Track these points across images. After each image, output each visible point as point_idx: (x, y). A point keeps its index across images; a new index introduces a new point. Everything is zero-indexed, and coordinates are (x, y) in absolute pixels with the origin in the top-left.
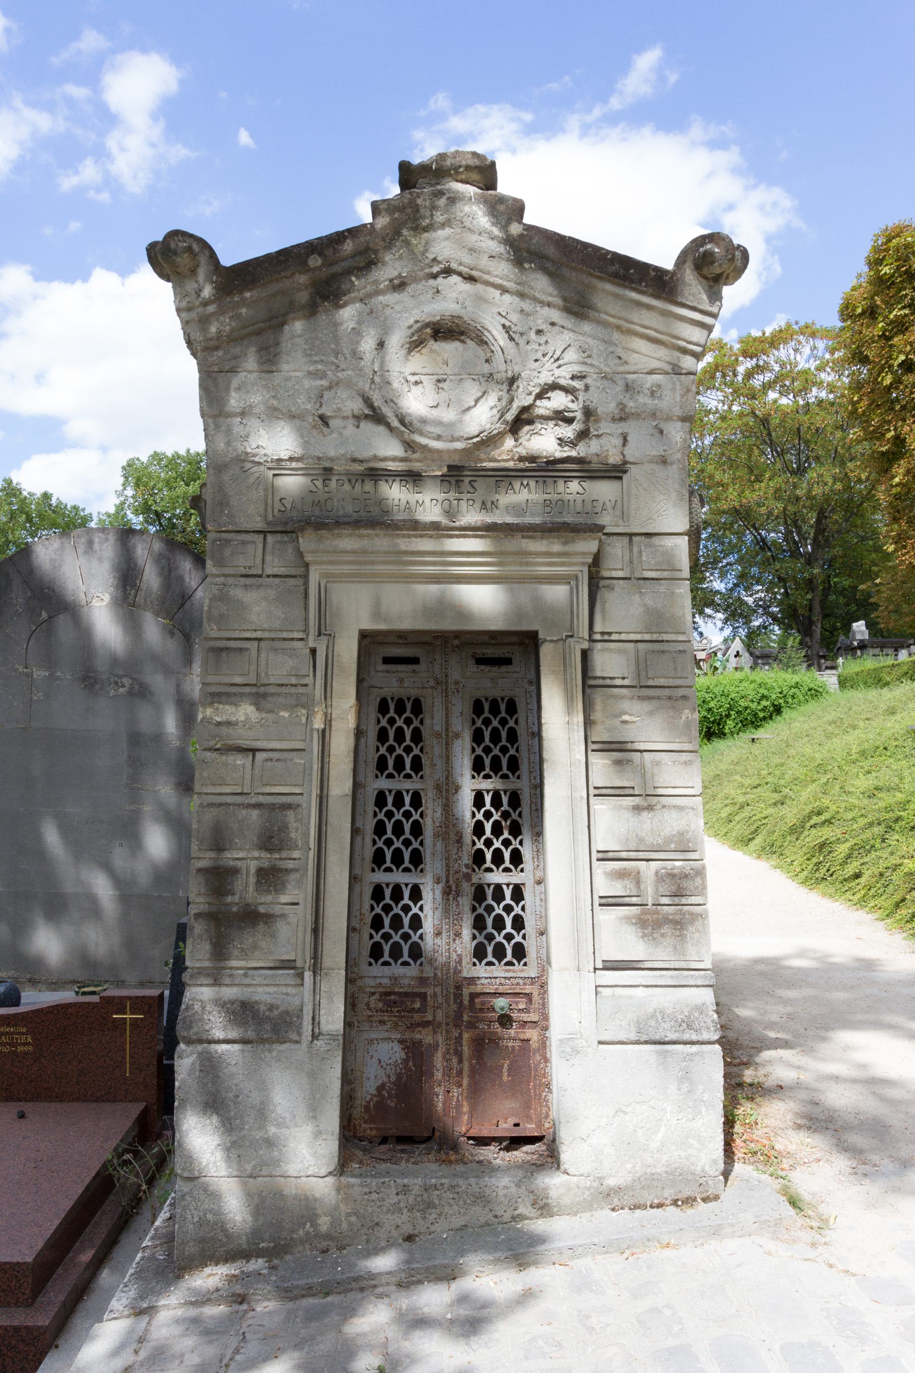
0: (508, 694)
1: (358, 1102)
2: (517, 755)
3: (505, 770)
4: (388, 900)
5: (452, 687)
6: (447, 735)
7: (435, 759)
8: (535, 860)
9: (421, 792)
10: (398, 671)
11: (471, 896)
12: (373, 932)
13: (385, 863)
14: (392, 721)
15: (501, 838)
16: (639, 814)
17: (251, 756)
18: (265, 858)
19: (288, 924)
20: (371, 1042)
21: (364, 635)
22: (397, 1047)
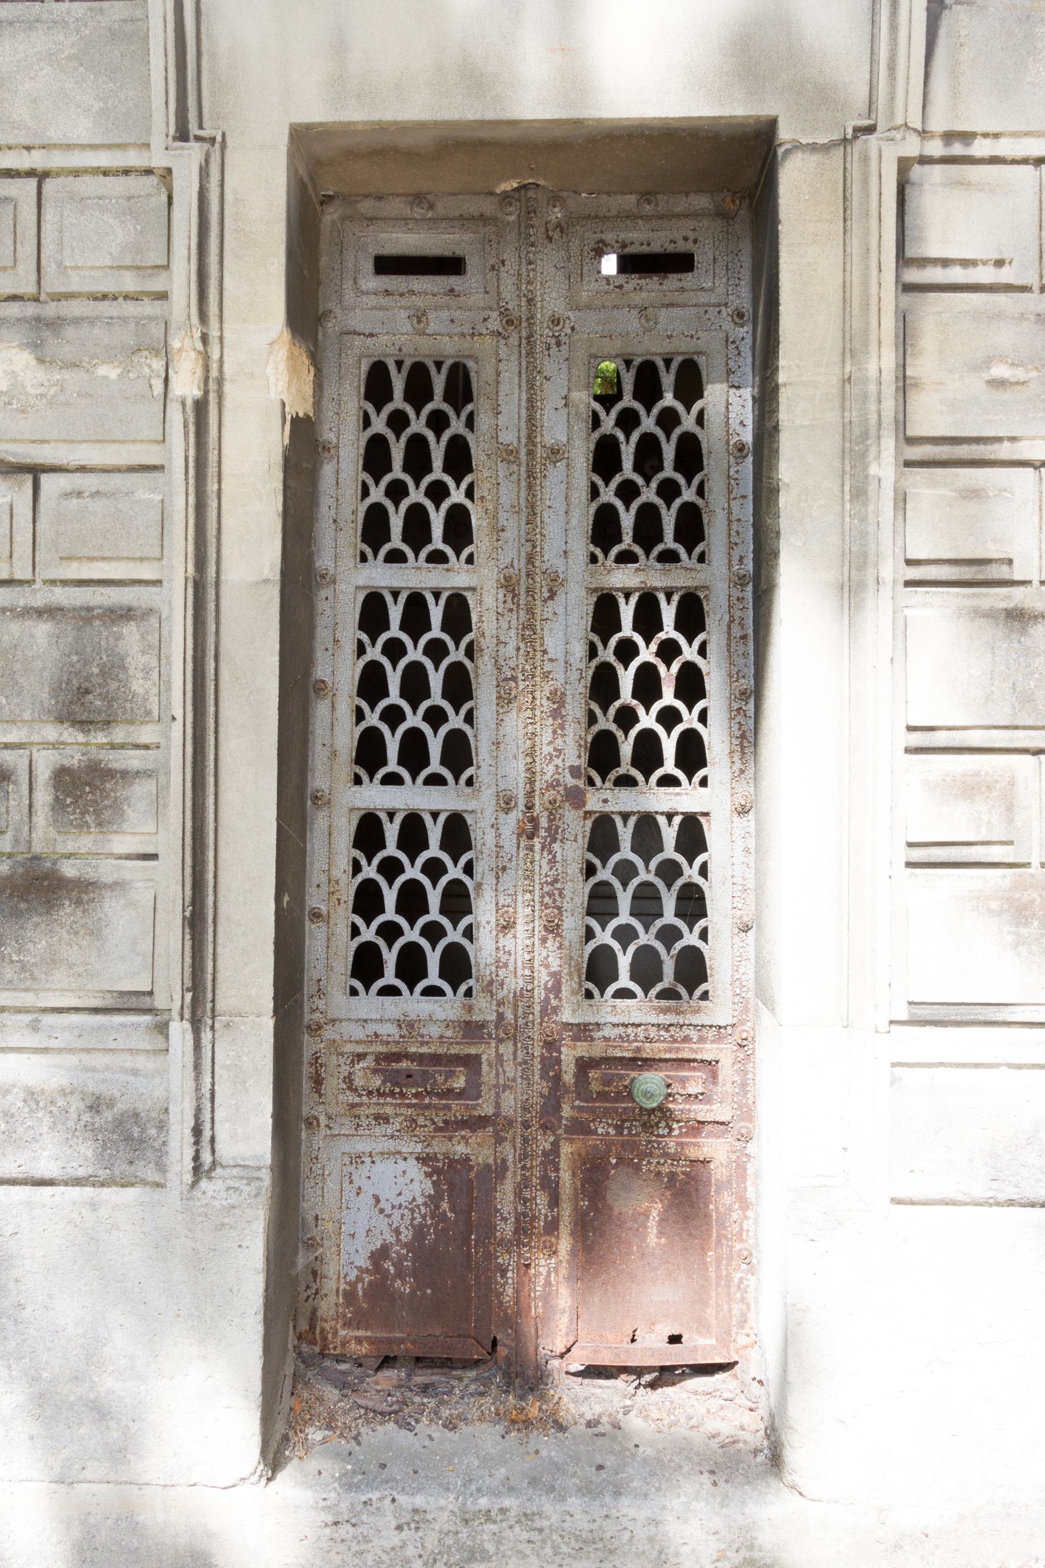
0: (683, 346)
1: (329, 1285)
2: (700, 502)
3: (669, 541)
4: (392, 849)
5: (543, 332)
6: (530, 453)
7: (503, 516)
8: (737, 757)
9: (468, 595)
10: (412, 292)
11: (583, 842)
12: (359, 922)
13: (384, 763)
14: (398, 422)
15: (657, 707)
16: (1023, 631)
17: (29, 483)
18: (74, 746)
19: (132, 905)
20: (357, 1159)
21: (302, 137)
22: (415, 1171)
